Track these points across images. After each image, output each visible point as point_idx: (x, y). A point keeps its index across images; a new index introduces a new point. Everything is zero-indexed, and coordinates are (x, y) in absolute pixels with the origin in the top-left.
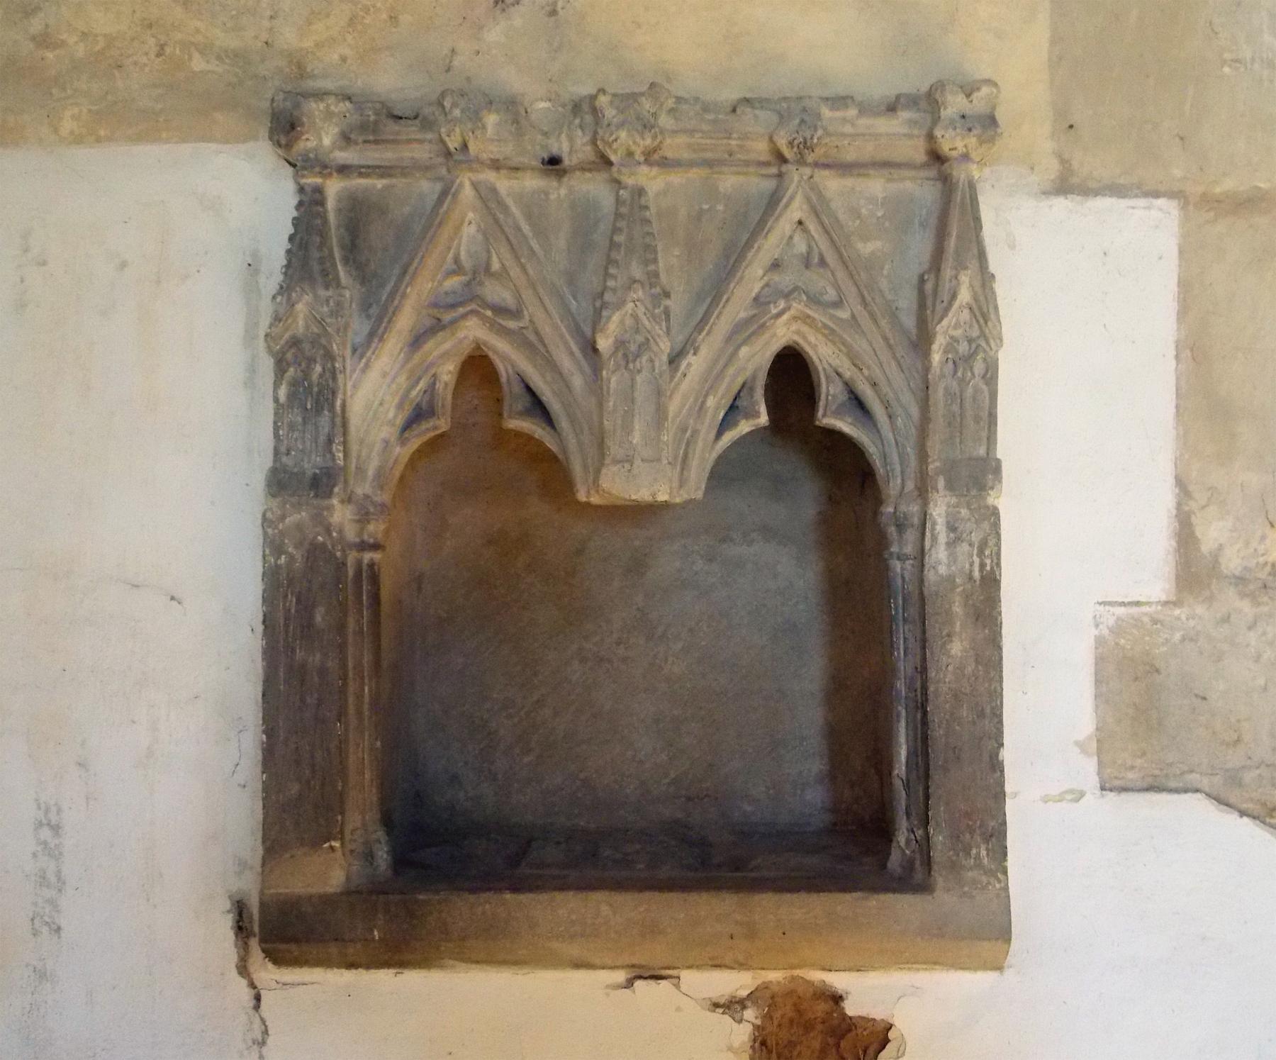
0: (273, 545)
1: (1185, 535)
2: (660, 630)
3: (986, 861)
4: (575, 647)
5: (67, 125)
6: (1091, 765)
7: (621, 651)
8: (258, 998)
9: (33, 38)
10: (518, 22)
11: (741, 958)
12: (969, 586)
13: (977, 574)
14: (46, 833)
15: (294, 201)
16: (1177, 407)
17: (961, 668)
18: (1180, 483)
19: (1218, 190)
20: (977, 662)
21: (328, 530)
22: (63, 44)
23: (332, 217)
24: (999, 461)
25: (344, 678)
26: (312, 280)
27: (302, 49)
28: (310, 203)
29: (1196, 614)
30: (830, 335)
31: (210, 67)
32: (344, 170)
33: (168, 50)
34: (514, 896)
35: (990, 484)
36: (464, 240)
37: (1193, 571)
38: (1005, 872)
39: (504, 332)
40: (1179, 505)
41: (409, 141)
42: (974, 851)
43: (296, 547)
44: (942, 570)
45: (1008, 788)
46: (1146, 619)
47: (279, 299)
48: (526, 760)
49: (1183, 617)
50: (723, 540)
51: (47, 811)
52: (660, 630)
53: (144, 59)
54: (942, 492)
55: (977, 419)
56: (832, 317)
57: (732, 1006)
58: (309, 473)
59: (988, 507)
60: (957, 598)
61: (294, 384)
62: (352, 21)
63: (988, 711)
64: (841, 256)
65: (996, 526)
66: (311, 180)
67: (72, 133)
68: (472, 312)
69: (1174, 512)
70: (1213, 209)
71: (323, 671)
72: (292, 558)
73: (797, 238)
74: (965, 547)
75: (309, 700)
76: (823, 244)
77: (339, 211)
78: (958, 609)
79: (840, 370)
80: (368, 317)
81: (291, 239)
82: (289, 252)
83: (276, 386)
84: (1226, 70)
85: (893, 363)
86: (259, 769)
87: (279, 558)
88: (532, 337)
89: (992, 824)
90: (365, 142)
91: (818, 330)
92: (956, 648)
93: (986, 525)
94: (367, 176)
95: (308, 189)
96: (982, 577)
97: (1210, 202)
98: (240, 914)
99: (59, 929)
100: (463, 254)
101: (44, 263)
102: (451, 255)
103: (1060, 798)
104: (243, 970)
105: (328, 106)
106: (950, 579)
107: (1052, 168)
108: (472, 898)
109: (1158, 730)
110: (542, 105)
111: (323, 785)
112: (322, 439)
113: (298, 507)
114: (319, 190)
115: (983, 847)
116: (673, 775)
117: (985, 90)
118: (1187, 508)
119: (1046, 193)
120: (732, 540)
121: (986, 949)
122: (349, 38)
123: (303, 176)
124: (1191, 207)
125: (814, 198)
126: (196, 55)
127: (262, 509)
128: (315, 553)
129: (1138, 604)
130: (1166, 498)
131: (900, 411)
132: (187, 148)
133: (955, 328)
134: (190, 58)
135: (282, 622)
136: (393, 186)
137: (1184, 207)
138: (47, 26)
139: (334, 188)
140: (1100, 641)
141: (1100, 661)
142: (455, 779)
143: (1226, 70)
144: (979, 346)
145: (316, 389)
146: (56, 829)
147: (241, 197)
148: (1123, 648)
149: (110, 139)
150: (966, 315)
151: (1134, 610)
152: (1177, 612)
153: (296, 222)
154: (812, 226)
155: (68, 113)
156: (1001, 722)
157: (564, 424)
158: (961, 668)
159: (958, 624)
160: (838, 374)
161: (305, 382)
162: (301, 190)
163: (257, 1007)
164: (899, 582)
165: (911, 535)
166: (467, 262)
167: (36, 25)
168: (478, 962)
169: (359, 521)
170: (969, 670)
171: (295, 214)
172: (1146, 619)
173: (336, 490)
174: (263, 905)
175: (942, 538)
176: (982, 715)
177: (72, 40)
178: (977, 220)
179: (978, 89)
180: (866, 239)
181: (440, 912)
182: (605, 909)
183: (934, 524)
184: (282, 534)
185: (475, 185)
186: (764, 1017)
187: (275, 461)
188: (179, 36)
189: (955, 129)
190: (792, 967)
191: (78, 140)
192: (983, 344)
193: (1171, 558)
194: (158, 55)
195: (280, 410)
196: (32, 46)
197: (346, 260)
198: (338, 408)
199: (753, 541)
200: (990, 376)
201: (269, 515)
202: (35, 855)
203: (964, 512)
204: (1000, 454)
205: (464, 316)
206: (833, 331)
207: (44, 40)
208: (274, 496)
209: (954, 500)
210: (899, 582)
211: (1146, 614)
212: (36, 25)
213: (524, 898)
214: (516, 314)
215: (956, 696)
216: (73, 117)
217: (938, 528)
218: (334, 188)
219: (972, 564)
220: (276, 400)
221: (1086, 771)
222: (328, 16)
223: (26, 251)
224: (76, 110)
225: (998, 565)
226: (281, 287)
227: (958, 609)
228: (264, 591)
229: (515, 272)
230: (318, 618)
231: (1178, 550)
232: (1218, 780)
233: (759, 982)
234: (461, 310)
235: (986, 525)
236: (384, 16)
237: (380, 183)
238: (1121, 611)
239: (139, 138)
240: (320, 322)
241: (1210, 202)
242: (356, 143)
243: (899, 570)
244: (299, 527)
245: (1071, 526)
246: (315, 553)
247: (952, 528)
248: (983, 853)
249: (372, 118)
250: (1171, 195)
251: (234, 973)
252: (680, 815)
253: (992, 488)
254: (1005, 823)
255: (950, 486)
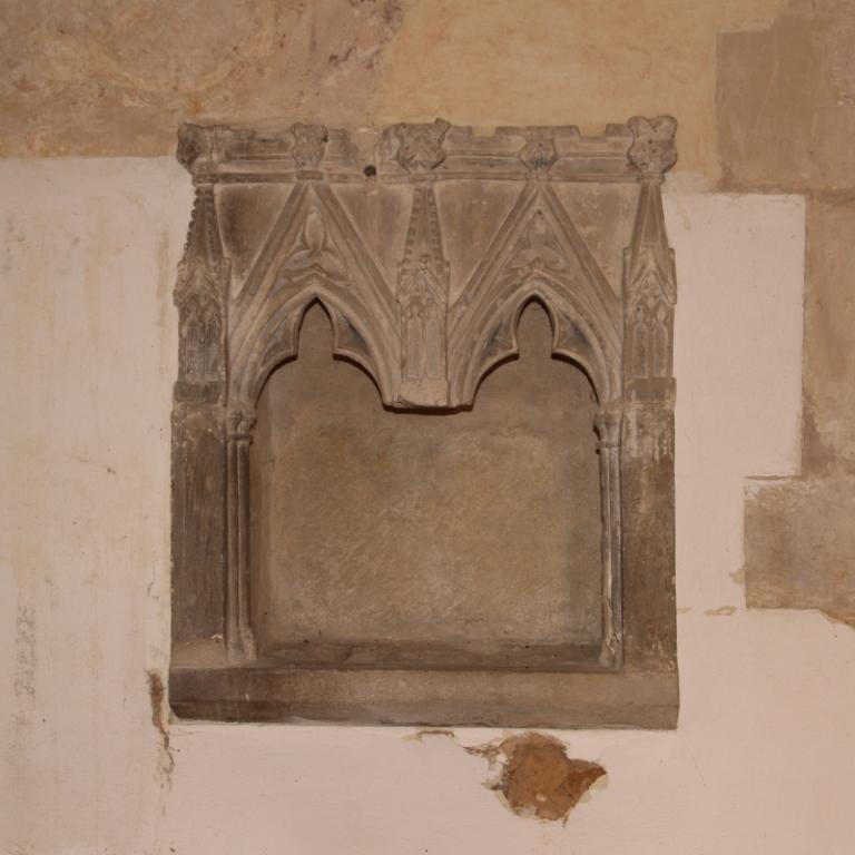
0: (179, 434)
1: (809, 432)
2: (447, 499)
3: (662, 653)
4: (385, 511)
5: (39, 144)
6: (740, 590)
7: (419, 513)
8: (167, 740)
9: (15, 83)
10: (346, 73)
11: (495, 719)
12: (652, 465)
13: (657, 457)
14: (24, 627)
15: (193, 197)
16: (804, 341)
17: (646, 521)
18: (807, 396)
19: (834, 188)
20: (657, 518)
21: (215, 425)
22: (35, 88)
23: (218, 208)
24: (674, 380)
25: (226, 525)
26: (205, 255)
27: (197, 92)
28: (203, 202)
29: (816, 486)
30: (561, 291)
31: (135, 104)
32: (227, 177)
33: (107, 93)
34: (340, 673)
35: (667, 395)
36: (308, 225)
37: (815, 456)
38: (675, 660)
39: (333, 288)
40: (805, 409)
41: (271, 158)
42: (653, 646)
43: (194, 436)
44: (634, 454)
45: (679, 604)
46: (780, 489)
47: (182, 266)
48: (351, 591)
49: (808, 487)
50: (493, 434)
51: (25, 611)
52: (447, 499)
53: (91, 99)
54: (634, 401)
55: (660, 350)
56: (562, 280)
57: (488, 752)
58: (203, 386)
59: (665, 411)
60: (644, 474)
61: (193, 324)
62: (232, 72)
63: (664, 550)
64: (567, 237)
65: (672, 423)
66: (206, 185)
67: (41, 149)
68: (314, 275)
69: (801, 414)
70: (828, 200)
71: (211, 521)
72: (191, 444)
73: (538, 224)
74: (649, 439)
75: (202, 539)
76: (555, 227)
77: (223, 204)
78: (644, 481)
79: (569, 315)
80: (242, 278)
81: (191, 225)
82: (189, 234)
83: (181, 325)
84: (840, 103)
85: (603, 311)
86: (169, 585)
87: (181, 443)
88: (353, 292)
89: (666, 627)
90: (241, 158)
91: (551, 286)
92: (643, 508)
93: (664, 424)
94: (242, 181)
95: (203, 191)
96: (661, 460)
97: (827, 195)
98: (154, 683)
99: (33, 692)
100: (307, 234)
101: (23, 239)
102: (299, 235)
103: (719, 612)
104: (157, 721)
105: (216, 134)
106: (639, 461)
107: (717, 172)
108: (312, 674)
109: (783, 563)
110: (363, 130)
111: (211, 597)
112: (211, 362)
113: (195, 408)
114: (211, 192)
115: (660, 643)
116: (455, 604)
117: (666, 123)
118: (810, 411)
119: (713, 191)
120: (501, 434)
121: (637, 683)
122: (230, 85)
123: (200, 182)
124: (815, 201)
125: (549, 197)
126: (126, 96)
127: (171, 409)
128: (206, 439)
129: (776, 478)
130: (795, 405)
131: (609, 343)
132: (118, 160)
133: (646, 288)
134: (121, 98)
135: (184, 486)
136: (259, 188)
137: (812, 198)
138: (24, 75)
139: (218, 189)
140: (748, 504)
141: (748, 518)
142: (298, 606)
143: (840, 103)
144: (660, 301)
145: (207, 328)
146: (31, 624)
147: (167, 196)
148: (766, 510)
149: (66, 154)
150: (652, 278)
151: (771, 483)
152: (803, 483)
153: (194, 214)
154: (548, 215)
155: (38, 136)
156: (673, 559)
157: (376, 352)
158: (646, 521)
159: (424, 360)
160: (567, 318)
161: (200, 323)
162: (198, 192)
163: (166, 746)
164: (608, 461)
165: (616, 431)
166: (310, 241)
167: (17, 74)
168: (315, 719)
169: (236, 419)
170: (651, 523)
171: (193, 208)
172: (780, 489)
173: (221, 397)
174: (172, 676)
175: (634, 432)
176: (660, 553)
177: (41, 85)
178: (661, 213)
179: (660, 123)
180: (585, 223)
181: (290, 683)
182: (402, 684)
183: (629, 422)
184: (184, 426)
185: (316, 188)
186: (510, 761)
187: (179, 377)
188: (114, 83)
189: (644, 150)
190: (530, 726)
191: (45, 154)
192: (664, 299)
193: (798, 446)
194: (100, 96)
195: (183, 342)
196: (14, 88)
197: (227, 239)
198: (222, 342)
199: (515, 434)
200: (669, 321)
201: (176, 414)
202: (17, 641)
203: (649, 415)
204: (676, 374)
205: (308, 278)
206: (562, 289)
207: (23, 85)
208: (179, 401)
209: (641, 407)
210: (608, 461)
211: (781, 485)
212: (17, 74)
213: (348, 674)
214: (342, 278)
215: (642, 541)
216: (42, 139)
217: (631, 425)
218: (218, 189)
219: (654, 450)
220: (180, 335)
221: (736, 594)
222: (215, 69)
223: (11, 230)
224: (44, 134)
225: (673, 450)
226: (185, 259)
227: (644, 481)
228: (173, 465)
229: (343, 247)
230: (209, 485)
231: (803, 440)
232: (830, 600)
233: (508, 736)
234: (307, 274)
235: (664, 424)
236: (254, 69)
237: (250, 186)
238: (762, 483)
239: (85, 154)
240: (212, 284)
241: (827, 195)
242: (235, 159)
243: (607, 455)
244: (195, 422)
245: (730, 425)
246: (206, 439)
247: (640, 426)
248: (660, 647)
249: (246, 141)
250: (800, 192)
251: (150, 722)
252: (460, 632)
253: (669, 398)
254: (675, 627)
255: (640, 396)
